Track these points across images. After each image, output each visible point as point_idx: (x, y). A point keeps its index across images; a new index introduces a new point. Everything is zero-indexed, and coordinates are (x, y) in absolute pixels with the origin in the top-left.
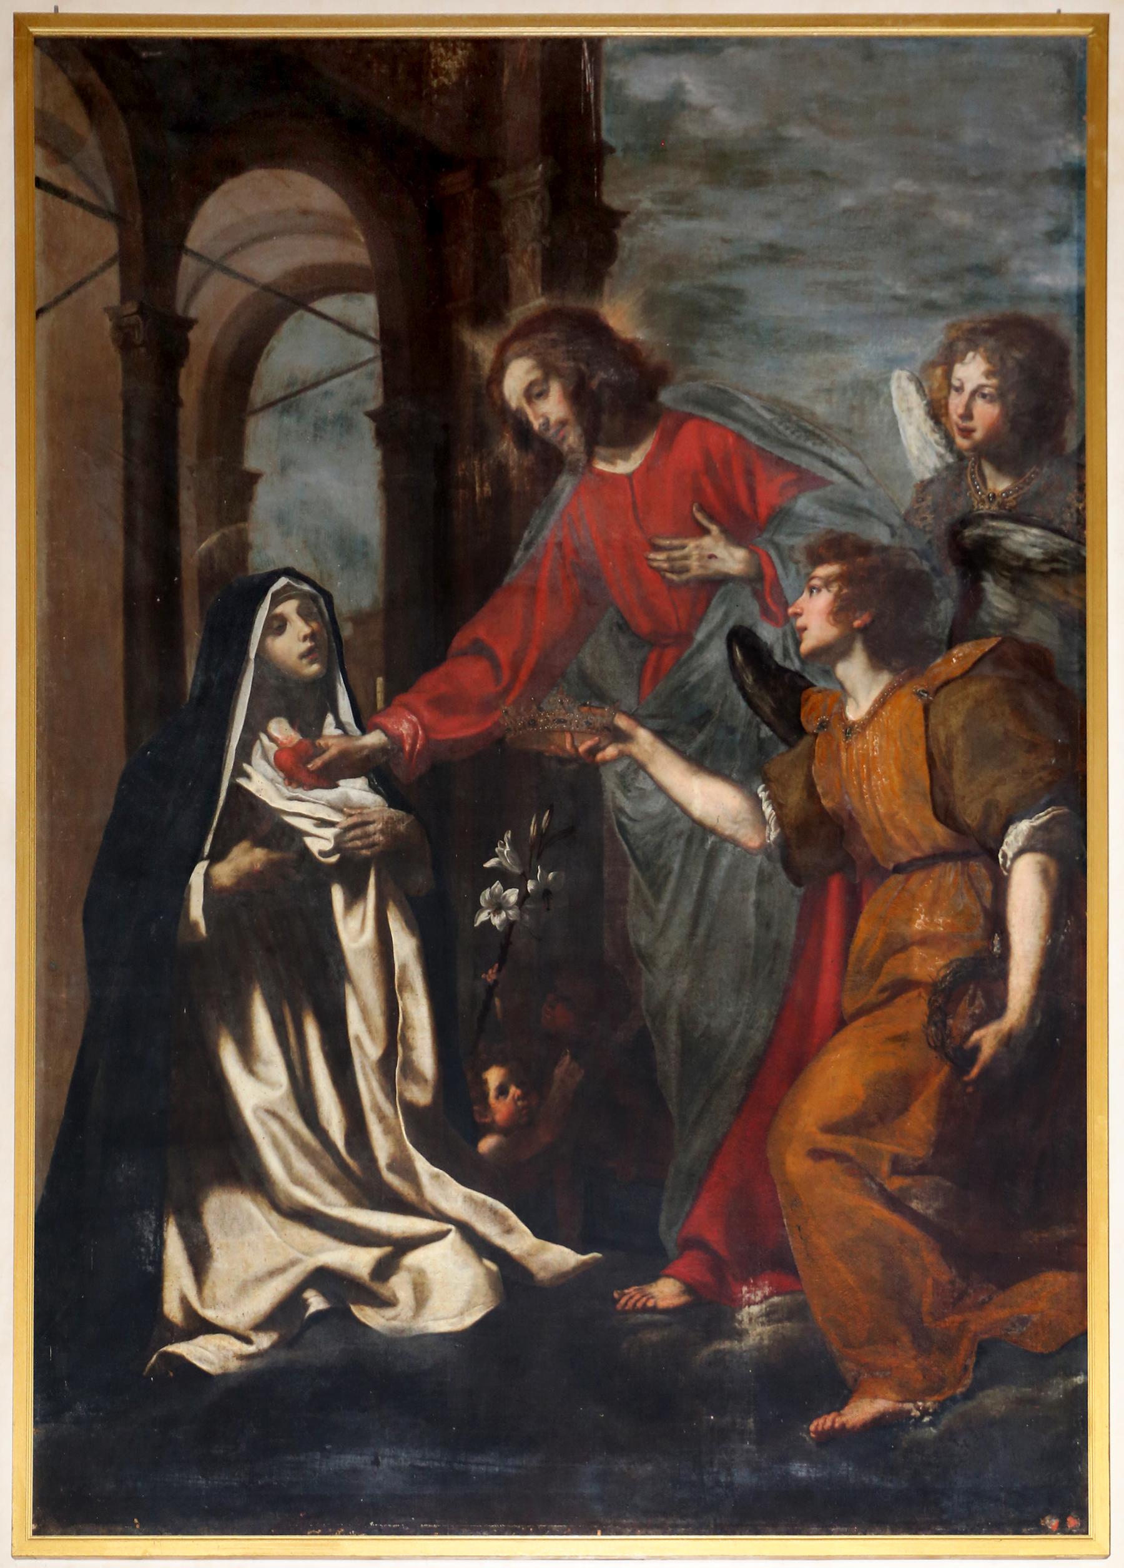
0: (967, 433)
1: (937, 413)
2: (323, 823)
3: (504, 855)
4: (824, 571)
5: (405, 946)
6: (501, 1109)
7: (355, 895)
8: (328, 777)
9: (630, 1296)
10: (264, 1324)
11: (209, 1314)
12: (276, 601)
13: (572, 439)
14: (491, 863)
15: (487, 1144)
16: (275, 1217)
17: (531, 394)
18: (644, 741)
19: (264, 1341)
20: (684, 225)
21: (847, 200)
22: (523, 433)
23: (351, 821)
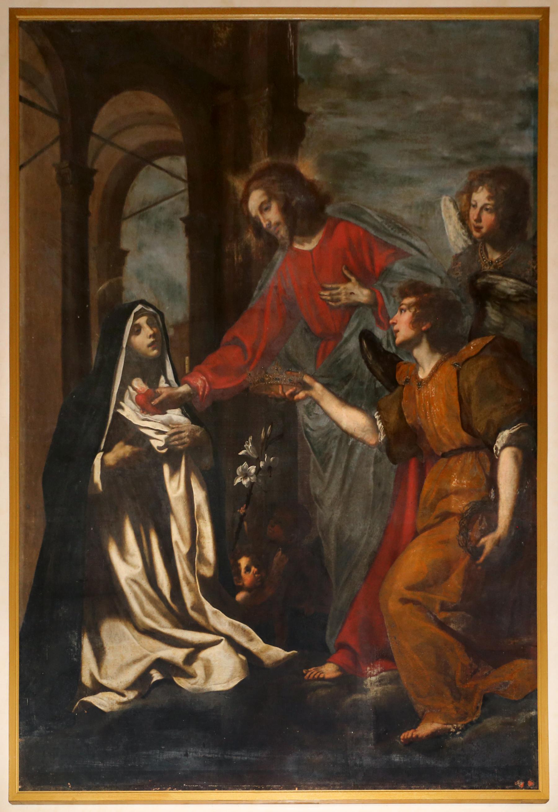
0: (478, 229)
1: (463, 218)
2: (160, 432)
3: (248, 449)
4: (408, 301)
6: (247, 578)
7: (175, 470)
8: (161, 409)
9: (311, 673)
10: (131, 687)
11: (104, 682)
13: (283, 232)
14: (242, 453)
15: (240, 596)
16: (136, 633)
17: (263, 208)
19: (131, 695)
21: (419, 107)
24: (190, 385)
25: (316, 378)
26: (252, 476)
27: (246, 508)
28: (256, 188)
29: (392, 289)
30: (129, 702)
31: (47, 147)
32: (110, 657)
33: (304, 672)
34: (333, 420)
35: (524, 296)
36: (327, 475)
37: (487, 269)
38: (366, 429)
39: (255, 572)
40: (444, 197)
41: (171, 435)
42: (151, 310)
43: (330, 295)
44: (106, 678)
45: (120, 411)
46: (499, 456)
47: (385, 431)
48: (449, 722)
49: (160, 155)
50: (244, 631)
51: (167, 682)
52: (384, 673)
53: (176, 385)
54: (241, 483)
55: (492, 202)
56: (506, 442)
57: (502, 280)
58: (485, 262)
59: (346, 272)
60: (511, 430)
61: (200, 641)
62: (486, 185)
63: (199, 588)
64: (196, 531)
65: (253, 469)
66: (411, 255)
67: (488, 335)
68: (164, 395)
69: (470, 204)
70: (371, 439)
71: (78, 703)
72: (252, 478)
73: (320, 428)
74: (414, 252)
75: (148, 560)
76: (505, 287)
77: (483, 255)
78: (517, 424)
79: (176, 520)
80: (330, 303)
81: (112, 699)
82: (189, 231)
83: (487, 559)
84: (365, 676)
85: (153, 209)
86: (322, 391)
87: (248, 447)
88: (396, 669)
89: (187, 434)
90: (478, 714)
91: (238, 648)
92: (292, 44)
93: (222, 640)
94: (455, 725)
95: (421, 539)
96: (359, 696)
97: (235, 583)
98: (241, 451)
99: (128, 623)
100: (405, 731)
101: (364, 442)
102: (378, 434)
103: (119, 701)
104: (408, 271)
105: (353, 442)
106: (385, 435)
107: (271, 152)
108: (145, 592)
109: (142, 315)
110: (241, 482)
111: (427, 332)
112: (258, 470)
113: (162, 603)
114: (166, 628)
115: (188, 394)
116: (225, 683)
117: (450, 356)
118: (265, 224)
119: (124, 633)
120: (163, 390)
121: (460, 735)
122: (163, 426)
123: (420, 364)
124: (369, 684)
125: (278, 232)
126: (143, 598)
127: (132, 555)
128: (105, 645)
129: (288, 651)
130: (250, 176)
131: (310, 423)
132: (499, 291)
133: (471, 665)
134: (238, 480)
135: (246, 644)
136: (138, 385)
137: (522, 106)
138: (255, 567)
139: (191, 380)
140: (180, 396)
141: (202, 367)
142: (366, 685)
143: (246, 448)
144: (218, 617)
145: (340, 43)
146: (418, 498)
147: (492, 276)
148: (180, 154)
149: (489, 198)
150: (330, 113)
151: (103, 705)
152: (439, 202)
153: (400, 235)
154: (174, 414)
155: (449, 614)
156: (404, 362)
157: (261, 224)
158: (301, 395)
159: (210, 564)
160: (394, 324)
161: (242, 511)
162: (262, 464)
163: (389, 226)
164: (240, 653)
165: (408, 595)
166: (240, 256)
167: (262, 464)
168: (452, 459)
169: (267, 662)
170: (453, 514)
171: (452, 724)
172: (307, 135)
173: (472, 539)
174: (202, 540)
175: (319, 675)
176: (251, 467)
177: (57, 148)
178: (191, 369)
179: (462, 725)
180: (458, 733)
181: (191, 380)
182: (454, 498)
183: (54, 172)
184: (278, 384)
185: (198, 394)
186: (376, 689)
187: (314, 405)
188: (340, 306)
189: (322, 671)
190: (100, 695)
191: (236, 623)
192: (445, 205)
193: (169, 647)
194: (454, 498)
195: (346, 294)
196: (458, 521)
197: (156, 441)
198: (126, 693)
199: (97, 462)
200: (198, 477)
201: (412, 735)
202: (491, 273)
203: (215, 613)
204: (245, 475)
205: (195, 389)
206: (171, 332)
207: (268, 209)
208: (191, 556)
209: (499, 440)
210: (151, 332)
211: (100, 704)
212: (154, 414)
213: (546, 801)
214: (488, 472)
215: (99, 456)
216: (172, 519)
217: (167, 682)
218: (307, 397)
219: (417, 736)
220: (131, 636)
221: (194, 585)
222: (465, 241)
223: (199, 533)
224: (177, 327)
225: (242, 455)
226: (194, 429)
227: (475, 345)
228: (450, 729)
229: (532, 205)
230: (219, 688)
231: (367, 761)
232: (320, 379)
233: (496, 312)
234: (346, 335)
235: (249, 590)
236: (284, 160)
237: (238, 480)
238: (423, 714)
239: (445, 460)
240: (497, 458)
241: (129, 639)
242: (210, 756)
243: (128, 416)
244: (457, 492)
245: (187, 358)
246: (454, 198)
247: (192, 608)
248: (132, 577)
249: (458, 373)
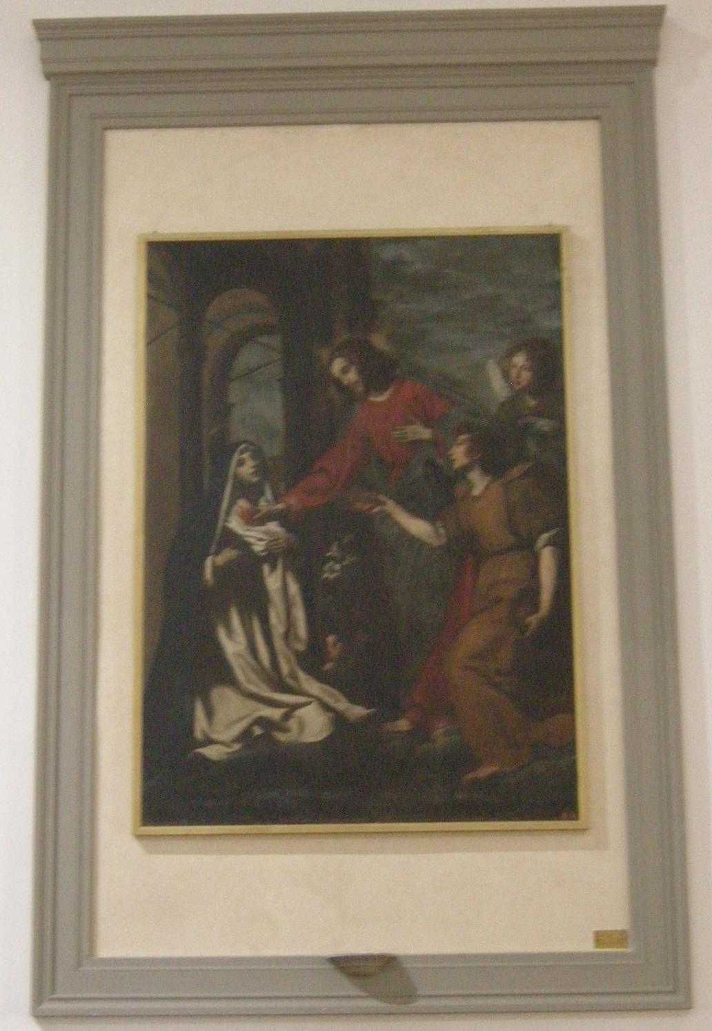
0: (518, 383)
1: (506, 375)
2: (261, 540)
3: (334, 551)
4: (462, 437)
5: (294, 588)
6: (334, 652)
7: (273, 568)
8: (262, 521)
9: (389, 726)
10: (237, 740)
11: (214, 736)
12: (242, 452)
13: (360, 388)
14: (328, 554)
15: (328, 666)
16: (240, 697)
17: (345, 371)
18: (391, 506)
19: (236, 747)
20: (404, 306)
21: (468, 296)
22: (337, 382)
23: (272, 538)
41: (271, 541)
51: (266, 736)
91: (326, 707)
199: (209, 563)
213: (583, 830)
217: (266, 736)
227: (516, 471)
230: (311, 740)
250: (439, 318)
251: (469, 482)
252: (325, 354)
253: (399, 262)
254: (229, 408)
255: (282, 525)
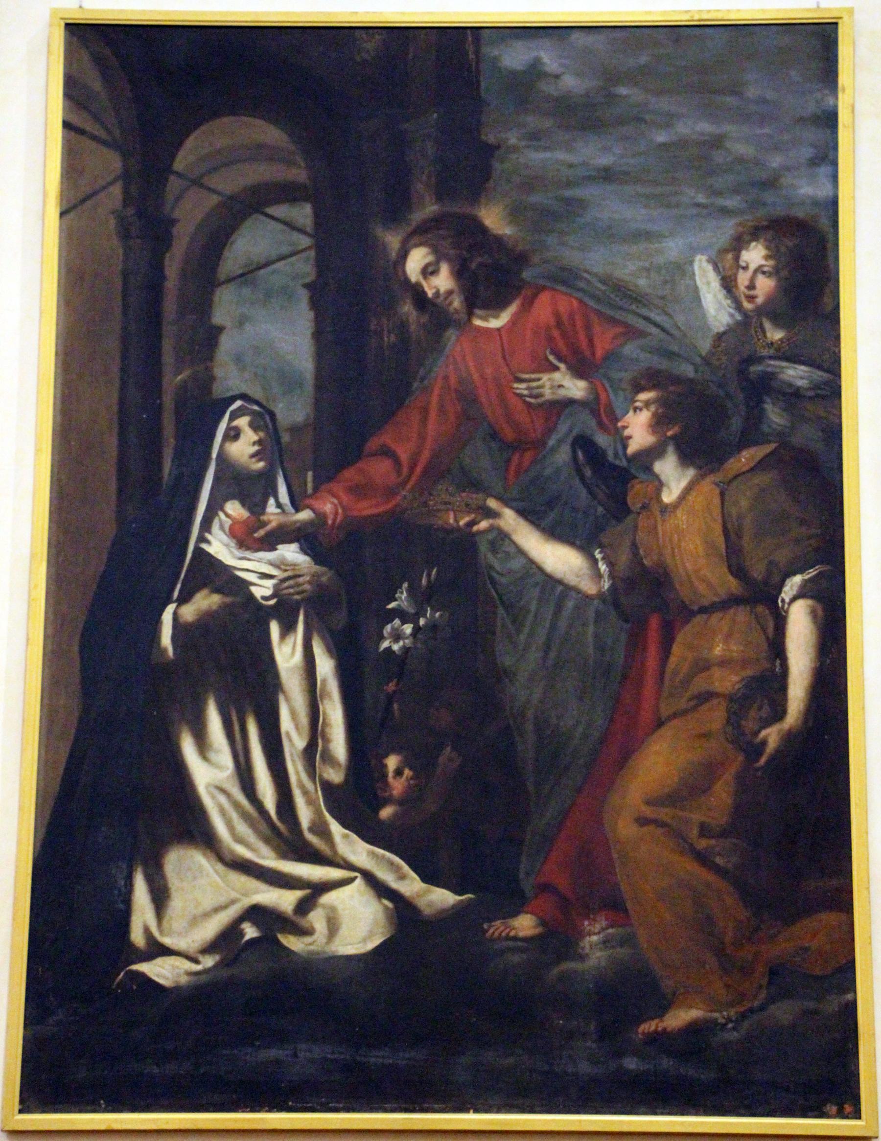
0: (751, 298)
1: (728, 284)
2: (265, 576)
3: (402, 599)
4: (643, 396)
5: (325, 666)
6: (398, 786)
7: (288, 628)
8: (270, 542)
9: (496, 928)
10: (209, 948)
11: (167, 941)
12: (234, 416)
13: (457, 303)
14: (391, 606)
15: (386, 813)
16: (220, 867)
17: (428, 271)
18: (509, 519)
19: (209, 961)
21: (661, 137)
23: (286, 574)
24: (313, 510)
25: (506, 503)
26: (407, 638)
27: (397, 684)
28: (416, 246)
29: (620, 380)
30: (206, 971)
31: (104, 188)
32: (177, 904)
33: (485, 926)
34: (532, 562)
35: (820, 389)
36: (522, 637)
37: (765, 352)
38: (581, 573)
39: (409, 778)
40: (698, 257)
42: (256, 408)
43: (528, 388)
44: (169, 934)
45: (204, 546)
46: (787, 612)
47: (612, 576)
48: (715, 1008)
49: (278, 201)
50: (392, 864)
52: (610, 931)
53: (289, 508)
54: (389, 649)
55: (771, 263)
56: (797, 591)
57: (787, 368)
58: (762, 343)
59: (551, 358)
60: (804, 574)
61: (320, 879)
62: (762, 240)
63: (322, 804)
64: (318, 717)
65: (408, 629)
66: (650, 334)
67: (770, 442)
68: (273, 524)
69: (738, 266)
70: (589, 587)
71: (122, 974)
72: (407, 641)
73: (510, 572)
74: (654, 330)
75: (242, 759)
76: (793, 377)
77: (758, 334)
78: (815, 566)
79: (287, 700)
80: (528, 399)
81: (177, 967)
82: (314, 304)
83: (772, 759)
84: (581, 935)
85: (262, 271)
86: (514, 520)
87: (401, 598)
88: (631, 925)
89: (308, 578)
90: (763, 995)
92: (472, 56)
93: (356, 878)
94: (725, 1013)
95: (666, 732)
96: (568, 965)
97: (379, 792)
98: (389, 603)
99: (208, 851)
100: (645, 1021)
101: (578, 591)
102: (601, 580)
103: (189, 970)
104: (643, 356)
105: (562, 592)
106: (611, 582)
107: (439, 198)
108: (237, 806)
109: (244, 415)
110: (391, 646)
111: (673, 438)
112: (417, 630)
113: (262, 821)
114: (268, 858)
115: (310, 523)
116: (360, 942)
117: (712, 471)
118: (430, 293)
119: (200, 866)
120: (272, 518)
121: (734, 1029)
122: (271, 568)
123: (664, 481)
124: (587, 946)
125: (450, 304)
126: (234, 816)
127: (218, 751)
128: (170, 885)
129: (460, 894)
130: (409, 229)
131: (497, 566)
132: (783, 382)
133: (748, 919)
134: (385, 644)
135: (394, 884)
136: (234, 511)
137: (811, 134)
138: (411, 769)
139: (317, 505)
140: (298, 525)
141: (333, 486)
142: (583, 948)
143: (398, 599)
144: (351, 843)
145: (543, 54)
146: (662, 674)
147: (772, 362)
148: (306, 200)
149: (767, 258)
150: (528, 147)
151: (164, 977)
152: (691, 263)
153: (634, 307)
154: (288, 551)
155: (713, 842)
156: (640, 480)
157: (424, 293)
158: (484, 525)
159: (340, 765)
160: (625, 427)
161: (391, 687)
162: (422, 622)
163: (617, 296)
164: (384, 897)
165: (648, 812)
166: (392, 335)
167: (422, 622)
168: (714, 615)
169: (427, 911)
170: (717, 695)
171: (721, 1012)
172: (495, 175)
173: (747, 732)
174: (327, 730)
175: (509, 932)
176: (405, 626)
177: (117, 190)
178: (316, 489)
179: (737, 1013)
180: (730, 1025)
181: (317, 505)
182: (717, 672)
183: (112, 222)
184: (448, 510)
185: (325, 523)
186: (599, 954)
187: (502, 540)
188: (541, 405)
189: (513, 926)
190: (159, 961)
191: (378, 852)
192: (700, 267)
193: (271, 888)
194: (717, 672)
195: (552, 387)
196: (725, 705)
197: (258, 588)
198: (201, 958)
199: (167, 617)
200: (323, 638)
201: (657, 1027)
202: (771, 358)
203: (345, 836)
204: (396, 637)
205: (321, 517)
206: (286, 438)
207: (435, 272)
208: (310, 752)
209: (786, 589)
210: (255, 438)
211: (158, 976)
212: (257, 550)
214: (771, 630)
215: (170, 609)
216: (281, 699)
218: (491, 528)
219: (664, 1030)
220: (211, 871)
221: (314, 796)
222: (732, 315)
223: (324, 720)
224: (294, 430)
225: (393, 609)
226: (319, 572)
227: (747, 457)
228: (716, 1019)
229: (832, 266)
230: (351, 950)
231: (585, 1068)
232: (514, 504)
233: (778, 411)
234: (551, 442)
235: (401, 802)
236: (455, 208)
237: (385, 644)
238: (674, 994)
239: (705, 616)
240: (784, 614)
241: (207, 875)
242: (333, 1057)
243: (216, 553)
244: (723, 663)
245: (310, 474)
246: (714, 258)
247: (311, 829)
248: (218, 784)
249: (722, 494)
250: (607, 175)
251: (657, 477)
252: (393, 240)
253: (535, 71)
254: (214, 334)
255: (304, 551)
